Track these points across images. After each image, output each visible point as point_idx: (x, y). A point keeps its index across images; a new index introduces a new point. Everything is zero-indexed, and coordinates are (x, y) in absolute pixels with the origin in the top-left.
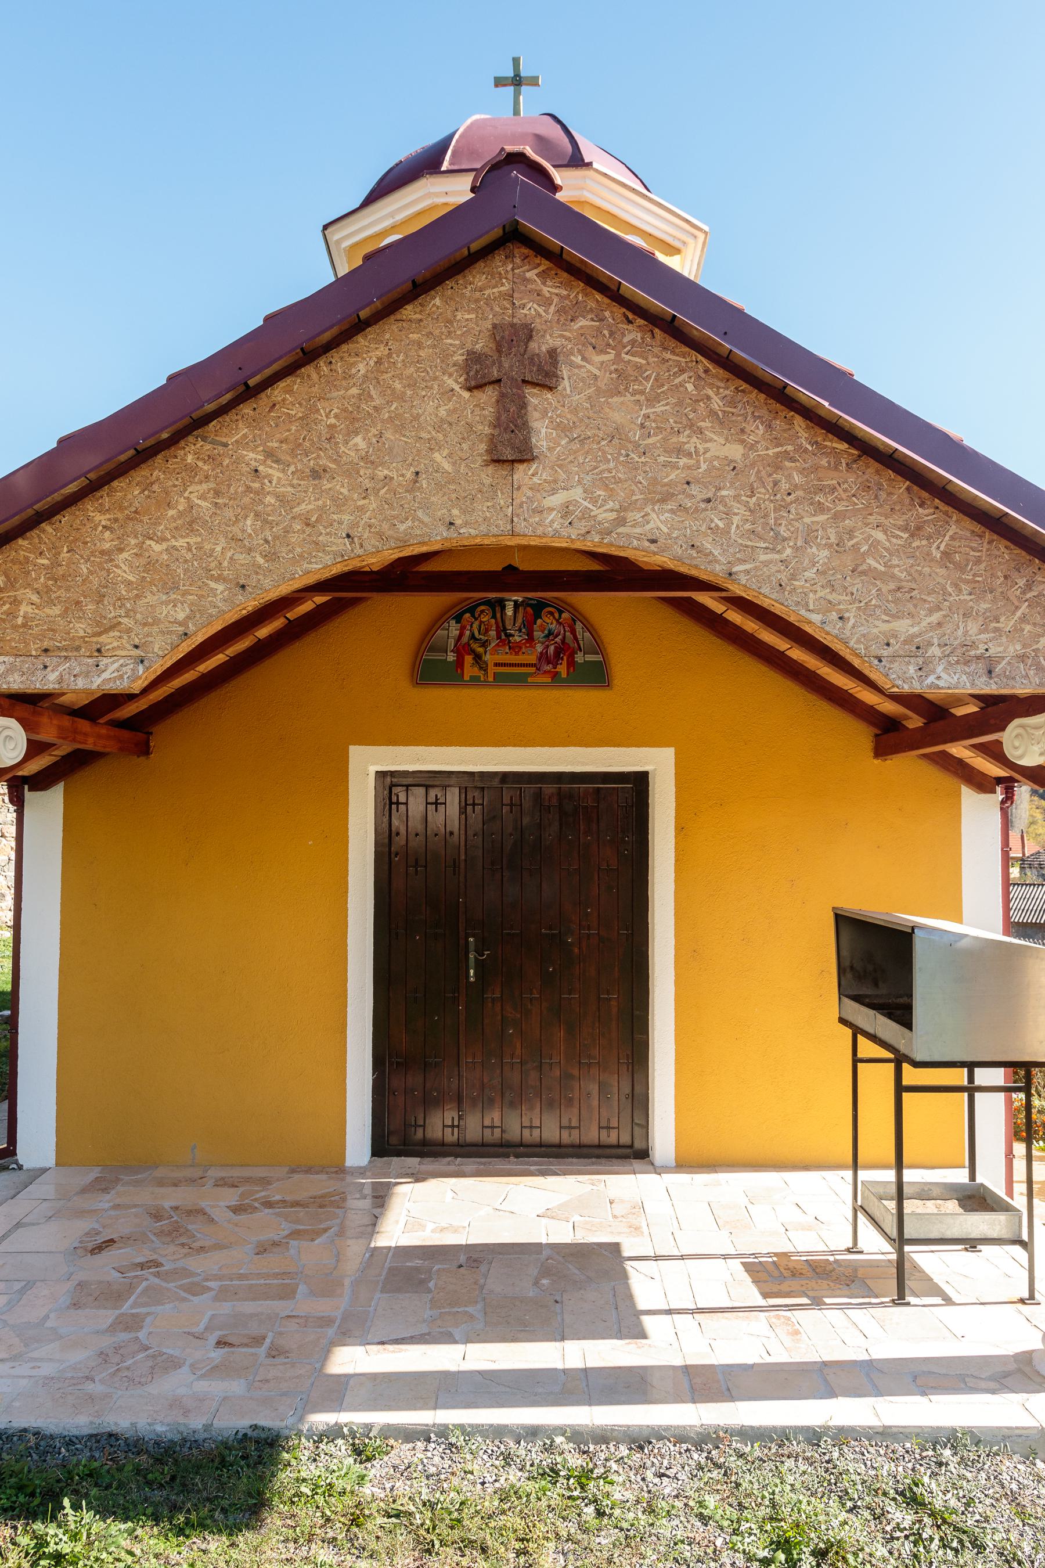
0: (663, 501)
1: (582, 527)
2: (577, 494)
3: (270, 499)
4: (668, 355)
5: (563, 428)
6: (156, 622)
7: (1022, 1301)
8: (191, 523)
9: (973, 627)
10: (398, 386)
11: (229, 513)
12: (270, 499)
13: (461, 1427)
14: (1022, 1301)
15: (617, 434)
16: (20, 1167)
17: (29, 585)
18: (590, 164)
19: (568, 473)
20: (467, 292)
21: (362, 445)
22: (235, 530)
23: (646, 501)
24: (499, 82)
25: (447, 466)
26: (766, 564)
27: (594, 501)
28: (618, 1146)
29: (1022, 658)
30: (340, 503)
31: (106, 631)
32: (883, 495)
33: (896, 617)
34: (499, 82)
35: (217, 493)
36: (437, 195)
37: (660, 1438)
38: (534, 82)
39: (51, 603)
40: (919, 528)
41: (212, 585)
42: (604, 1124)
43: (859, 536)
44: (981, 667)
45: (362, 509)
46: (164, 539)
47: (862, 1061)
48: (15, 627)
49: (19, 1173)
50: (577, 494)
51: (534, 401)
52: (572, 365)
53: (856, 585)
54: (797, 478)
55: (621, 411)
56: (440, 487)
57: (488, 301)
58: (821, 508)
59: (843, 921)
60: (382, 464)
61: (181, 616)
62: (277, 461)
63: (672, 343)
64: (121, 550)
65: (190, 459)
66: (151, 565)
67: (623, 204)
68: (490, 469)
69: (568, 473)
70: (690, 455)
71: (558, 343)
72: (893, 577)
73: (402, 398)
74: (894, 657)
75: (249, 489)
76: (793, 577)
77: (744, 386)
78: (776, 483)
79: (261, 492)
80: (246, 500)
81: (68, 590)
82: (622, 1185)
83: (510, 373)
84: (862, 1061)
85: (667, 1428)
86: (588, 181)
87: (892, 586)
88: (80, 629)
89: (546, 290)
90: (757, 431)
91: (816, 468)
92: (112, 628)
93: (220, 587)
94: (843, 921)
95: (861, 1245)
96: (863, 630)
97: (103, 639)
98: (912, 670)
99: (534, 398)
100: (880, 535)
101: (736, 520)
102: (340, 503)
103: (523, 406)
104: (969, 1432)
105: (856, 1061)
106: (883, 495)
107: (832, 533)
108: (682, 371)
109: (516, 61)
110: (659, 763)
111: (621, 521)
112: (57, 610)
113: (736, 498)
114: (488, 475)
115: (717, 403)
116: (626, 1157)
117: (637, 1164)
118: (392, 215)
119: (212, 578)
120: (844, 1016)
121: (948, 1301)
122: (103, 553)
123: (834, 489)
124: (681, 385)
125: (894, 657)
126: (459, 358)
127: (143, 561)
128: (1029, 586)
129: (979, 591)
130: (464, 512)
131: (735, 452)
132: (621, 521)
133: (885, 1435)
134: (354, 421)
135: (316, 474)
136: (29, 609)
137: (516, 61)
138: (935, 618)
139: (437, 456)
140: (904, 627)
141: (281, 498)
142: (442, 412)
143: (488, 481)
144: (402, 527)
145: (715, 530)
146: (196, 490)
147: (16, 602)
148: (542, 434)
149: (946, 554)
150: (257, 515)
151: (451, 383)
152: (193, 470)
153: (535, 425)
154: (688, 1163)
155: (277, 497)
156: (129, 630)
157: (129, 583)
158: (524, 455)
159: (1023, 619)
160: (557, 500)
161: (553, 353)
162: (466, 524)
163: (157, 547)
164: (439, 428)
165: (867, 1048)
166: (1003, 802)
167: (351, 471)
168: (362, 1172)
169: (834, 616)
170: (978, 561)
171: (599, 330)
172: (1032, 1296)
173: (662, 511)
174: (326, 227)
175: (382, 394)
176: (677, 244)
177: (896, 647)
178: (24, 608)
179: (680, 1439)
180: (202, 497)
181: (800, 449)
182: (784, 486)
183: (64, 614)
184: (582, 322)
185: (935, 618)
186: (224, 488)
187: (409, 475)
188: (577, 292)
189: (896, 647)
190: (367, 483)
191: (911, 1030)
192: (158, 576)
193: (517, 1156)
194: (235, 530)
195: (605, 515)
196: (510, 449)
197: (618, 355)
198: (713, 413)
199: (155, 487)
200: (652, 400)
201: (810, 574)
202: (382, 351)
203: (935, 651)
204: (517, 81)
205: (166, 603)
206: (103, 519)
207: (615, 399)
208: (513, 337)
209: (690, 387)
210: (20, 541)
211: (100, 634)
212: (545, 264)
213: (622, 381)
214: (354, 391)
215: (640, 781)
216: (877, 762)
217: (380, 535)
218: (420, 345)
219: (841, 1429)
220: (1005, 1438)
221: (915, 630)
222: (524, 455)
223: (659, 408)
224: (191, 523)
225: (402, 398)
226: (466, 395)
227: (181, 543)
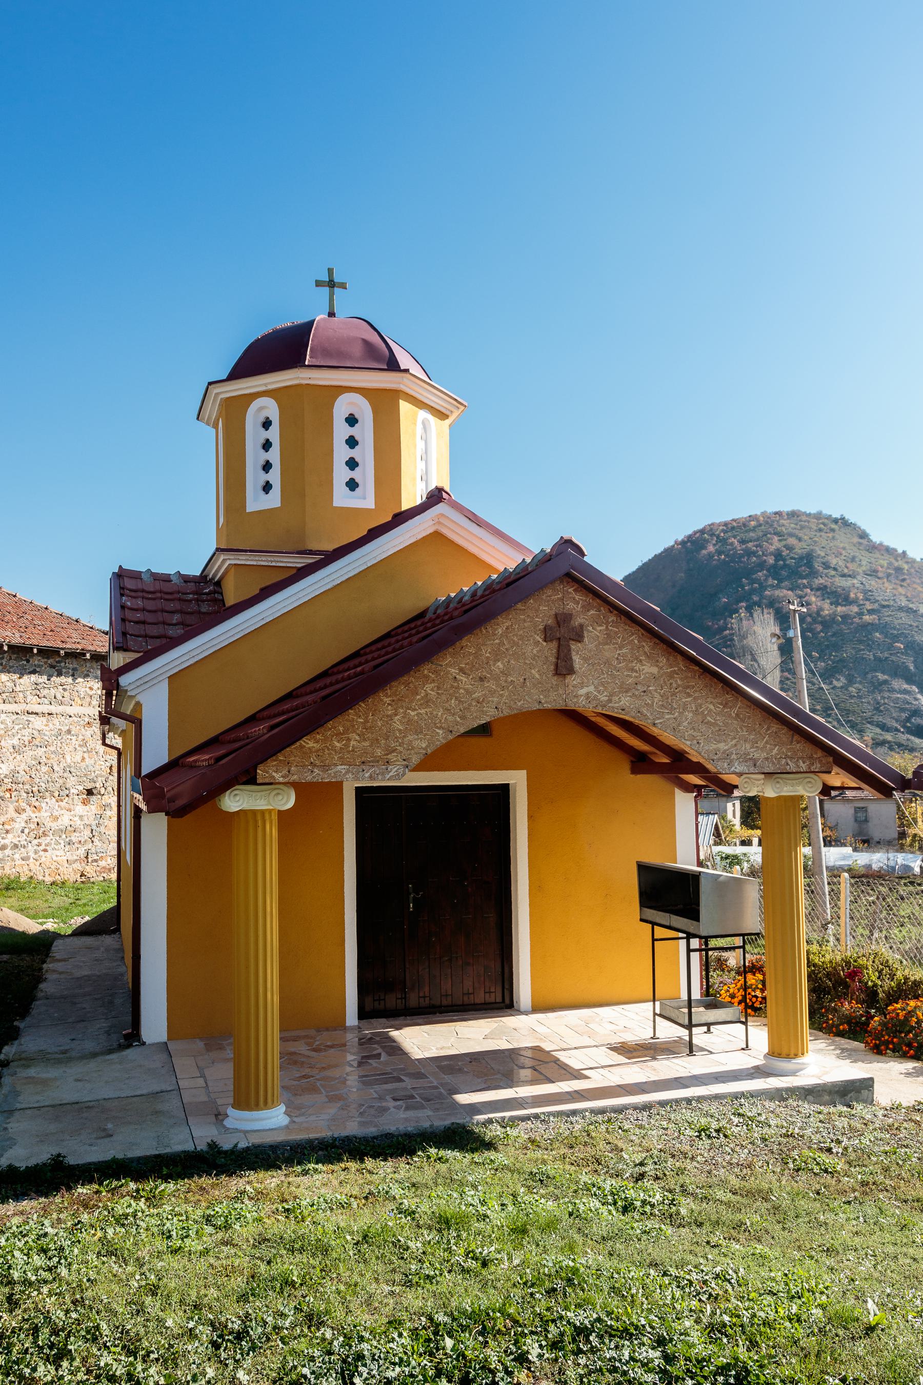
0: (626, 692)
1: (594, 703)
2: (591, 689)
3: (462, 691)
4: (627, 627)
5: (586, 659)
6: (413, 748)
7: (743, 1049)
8: (427, 702)
9: (748, 746)
10: (515, 639)
11: (444, 698)
12: (462, 691)
13: (544, 1113)
14: (743, 1049)
15: (607, 662)
16: (144, 1044)
17: (354, 732)
18: (407, 371)
19: (588, 679)
20: (544, 597)
21: (501, 666)
22: (447, 705)
23: (620, 692)
24: (319, 284)
25: (537, 676)
26: (668, 719)
27: (599, 692)
28: (496, 1003)
29: (767, 759)
30: (492, 693)
31: (391, 753)
32: (713, 689)
33: (719, 742)
34: (319, 284)
35: (439, 688)
36: (302, 378)
37: (627, 1109)
38: (343, 286)
39: (365, 740)
40: (726, 704)
41: (438, 731)
42: (487, 990)
43: (704, 707)
44: (750, 763)
45: (502, 695)
46: (415, 710)
47: (657, 940)
48: (349, 752)
49: (143, 1048)
50: (591, 689)
51: (573, 647)
52: (589, 631)
53: (703, 728)
54: (679, 682)
55: (609, 652)
56: (534, 685)
57: (553, 601)
58: (689, 695)
59: (643, 869)
60: (510, 675)
61: (424, 745)
62: (465, 673)
63: (629, 622)
64: (396, 715)
65: (426, 672)
66: (410, 722)
67: (425, 394)
68: (556, 678)
69: (588, 679)
70: (636, 672)
71: (582, 621)
72: (717, 725)
73: (517, 645)
74: (719, 759)
75: (452, 686)
76: (679, 725)
77: (658, 641)
78: (671, 684)
79: (458, 688)
80: (451, 691)
81: (372, 733)
82: (510, 1021)
83: (562, 635)
84: (657, 940)
85: (629, 1105)
86: (405, 380)
87: (717, 729)
88: (379, 752)
89: (577, 597)
90: (663, 661)
91: (687, 677)
92: (394, 751)
93: (441, 732)
94: (643, 869)
95: (657, 1036)
96: (706, 748)
97: (389, 756)
98: (726, 765)
99: (574, 646)
100: (712, 707)
101: (656, 700)
102: (492, 693)
103: (569, 650)
104: (748, 1092)
105: (654, 940)
106: (713, 689)
107: (693, 705)
108: (633, 634)
109: (330, 271)
110: (517, 780)
111: (610, 701)
112: (367, 744)
113: (656, 690)
114: (554, 680)
115: (647, 649)
116: (501, 1008)
117: (509, 1011)
118: (265, 385)
119: (437, 728)
120: (644, 917)
121: (711, 1053)
122: (388, 716)
123: (693, 687)
124: (632, 640)
125: (719, 759)
126: (541, 627)
127: (406, 720)
128: (768, 729)
129: (751, 730)
130: (545, 697)
131: (655, 670)
132: (610, 701)
133: (717, 1097)
134: (497, 655)
135: (481, 679)
136: (355, 743)
137: (330, 271)
138: (734, 742)
139: (533, 671)
140: (722, 746)
141: (467, 691)
142: (535, 652)
143: (555, 683)
144: (519, 704)
145: (647, 705)
146: (428, 687)
147: (349, 740)
148: (577, 660)
149: (737, 714)
150: (456, 698)
151: (538, 638)
152: (427, 677)
153: (574, 658)
154: (538, 1008)
155: (465, 689)
156: (401, 752)
157: (400, 730)
158: (571, 671)
159: (767, 743)
160: (583, 691)
161: (581, 626)
162: (546, 702)
163: (412, 713)
164: (534, 659)
165: (660, 932)
166: (696, 797)
167: (497, 679)
168: (352, 1028)
169: (695, 742)
170: (749, 718)
171: (599, 616)
172: (747, 1047)
173: (627, 696)
174: (210, 384)
175: (509, 642)
176: (447, 413)
177: (719, 755)
178: (352, 743)
179: (635, 1108)
180: (432, 690)
181: (680, 669)
182: (674, 685)
183: (371, 746)
184: (592, 612)
185: (734, 742)
186: (441, 686)
187: (522, 680)
188: (589, 599)
189: (719, 755)
190: (504, 684)
191: (698, 920)
192: (414, 727)
193: (441, 1013)
194: (447, 705)
195: (603, 698)
196: (563, 667)
197: (607, 627)
198: (645, 653)
199: (411, 685)
200: (621, 648)
201: (685, 724)
202: (508, 623)
203: (734, 756)
204: (331, 284)
205: (417, 739)
206: (388, 700)
207: (606, 647)
208: (562, 619)
209: (636, 642)
210: (350, 711)
211: (387, 755)
212: (576, 586)
213: (609, 637)
214: (497, 641)
215: (504, 789)
216: (632, 776)
217: (510, 707)
218: (525, 621)
219: (699, 1097)
220: (762, 1094)
221: (726, 747)
222: (571, 671)
223: (624, 651)
224: (427, 702)
225: (517, 645)
226: (545, 644)
227: (423, 711)
